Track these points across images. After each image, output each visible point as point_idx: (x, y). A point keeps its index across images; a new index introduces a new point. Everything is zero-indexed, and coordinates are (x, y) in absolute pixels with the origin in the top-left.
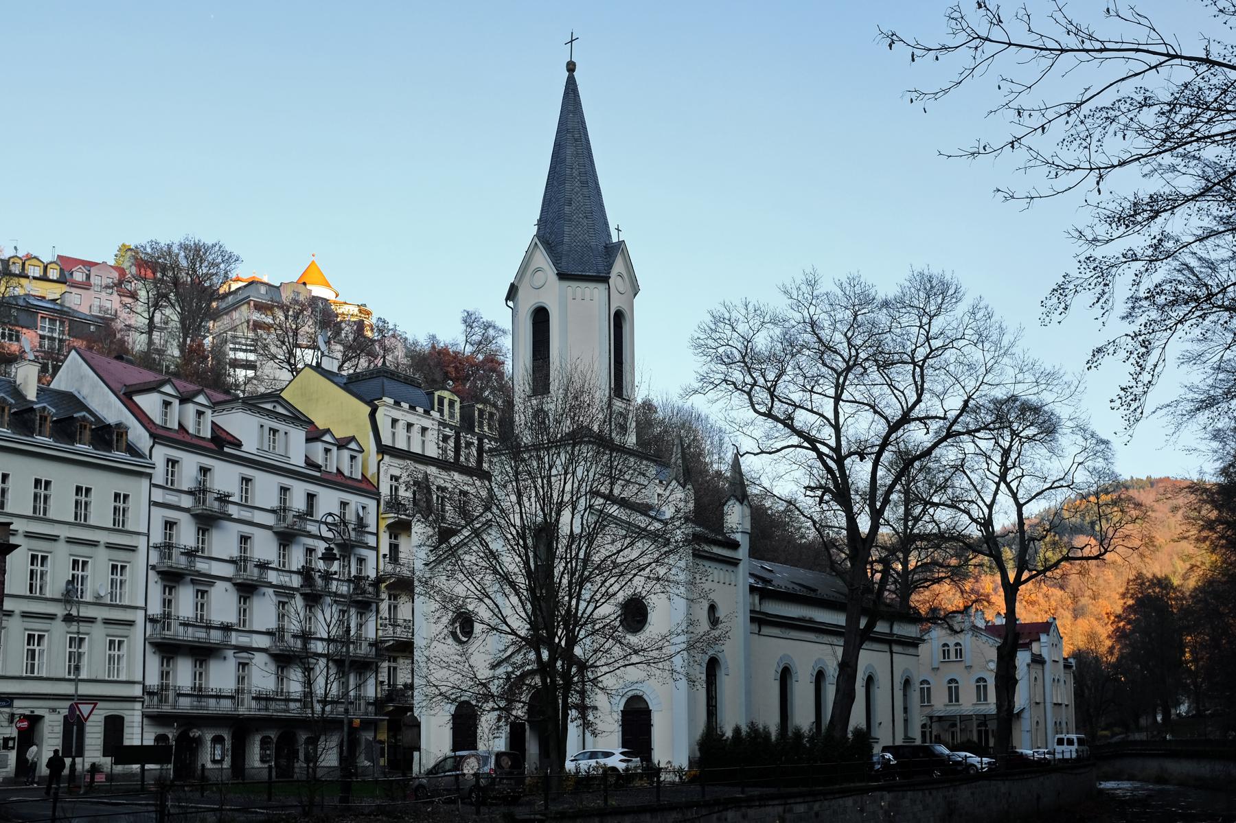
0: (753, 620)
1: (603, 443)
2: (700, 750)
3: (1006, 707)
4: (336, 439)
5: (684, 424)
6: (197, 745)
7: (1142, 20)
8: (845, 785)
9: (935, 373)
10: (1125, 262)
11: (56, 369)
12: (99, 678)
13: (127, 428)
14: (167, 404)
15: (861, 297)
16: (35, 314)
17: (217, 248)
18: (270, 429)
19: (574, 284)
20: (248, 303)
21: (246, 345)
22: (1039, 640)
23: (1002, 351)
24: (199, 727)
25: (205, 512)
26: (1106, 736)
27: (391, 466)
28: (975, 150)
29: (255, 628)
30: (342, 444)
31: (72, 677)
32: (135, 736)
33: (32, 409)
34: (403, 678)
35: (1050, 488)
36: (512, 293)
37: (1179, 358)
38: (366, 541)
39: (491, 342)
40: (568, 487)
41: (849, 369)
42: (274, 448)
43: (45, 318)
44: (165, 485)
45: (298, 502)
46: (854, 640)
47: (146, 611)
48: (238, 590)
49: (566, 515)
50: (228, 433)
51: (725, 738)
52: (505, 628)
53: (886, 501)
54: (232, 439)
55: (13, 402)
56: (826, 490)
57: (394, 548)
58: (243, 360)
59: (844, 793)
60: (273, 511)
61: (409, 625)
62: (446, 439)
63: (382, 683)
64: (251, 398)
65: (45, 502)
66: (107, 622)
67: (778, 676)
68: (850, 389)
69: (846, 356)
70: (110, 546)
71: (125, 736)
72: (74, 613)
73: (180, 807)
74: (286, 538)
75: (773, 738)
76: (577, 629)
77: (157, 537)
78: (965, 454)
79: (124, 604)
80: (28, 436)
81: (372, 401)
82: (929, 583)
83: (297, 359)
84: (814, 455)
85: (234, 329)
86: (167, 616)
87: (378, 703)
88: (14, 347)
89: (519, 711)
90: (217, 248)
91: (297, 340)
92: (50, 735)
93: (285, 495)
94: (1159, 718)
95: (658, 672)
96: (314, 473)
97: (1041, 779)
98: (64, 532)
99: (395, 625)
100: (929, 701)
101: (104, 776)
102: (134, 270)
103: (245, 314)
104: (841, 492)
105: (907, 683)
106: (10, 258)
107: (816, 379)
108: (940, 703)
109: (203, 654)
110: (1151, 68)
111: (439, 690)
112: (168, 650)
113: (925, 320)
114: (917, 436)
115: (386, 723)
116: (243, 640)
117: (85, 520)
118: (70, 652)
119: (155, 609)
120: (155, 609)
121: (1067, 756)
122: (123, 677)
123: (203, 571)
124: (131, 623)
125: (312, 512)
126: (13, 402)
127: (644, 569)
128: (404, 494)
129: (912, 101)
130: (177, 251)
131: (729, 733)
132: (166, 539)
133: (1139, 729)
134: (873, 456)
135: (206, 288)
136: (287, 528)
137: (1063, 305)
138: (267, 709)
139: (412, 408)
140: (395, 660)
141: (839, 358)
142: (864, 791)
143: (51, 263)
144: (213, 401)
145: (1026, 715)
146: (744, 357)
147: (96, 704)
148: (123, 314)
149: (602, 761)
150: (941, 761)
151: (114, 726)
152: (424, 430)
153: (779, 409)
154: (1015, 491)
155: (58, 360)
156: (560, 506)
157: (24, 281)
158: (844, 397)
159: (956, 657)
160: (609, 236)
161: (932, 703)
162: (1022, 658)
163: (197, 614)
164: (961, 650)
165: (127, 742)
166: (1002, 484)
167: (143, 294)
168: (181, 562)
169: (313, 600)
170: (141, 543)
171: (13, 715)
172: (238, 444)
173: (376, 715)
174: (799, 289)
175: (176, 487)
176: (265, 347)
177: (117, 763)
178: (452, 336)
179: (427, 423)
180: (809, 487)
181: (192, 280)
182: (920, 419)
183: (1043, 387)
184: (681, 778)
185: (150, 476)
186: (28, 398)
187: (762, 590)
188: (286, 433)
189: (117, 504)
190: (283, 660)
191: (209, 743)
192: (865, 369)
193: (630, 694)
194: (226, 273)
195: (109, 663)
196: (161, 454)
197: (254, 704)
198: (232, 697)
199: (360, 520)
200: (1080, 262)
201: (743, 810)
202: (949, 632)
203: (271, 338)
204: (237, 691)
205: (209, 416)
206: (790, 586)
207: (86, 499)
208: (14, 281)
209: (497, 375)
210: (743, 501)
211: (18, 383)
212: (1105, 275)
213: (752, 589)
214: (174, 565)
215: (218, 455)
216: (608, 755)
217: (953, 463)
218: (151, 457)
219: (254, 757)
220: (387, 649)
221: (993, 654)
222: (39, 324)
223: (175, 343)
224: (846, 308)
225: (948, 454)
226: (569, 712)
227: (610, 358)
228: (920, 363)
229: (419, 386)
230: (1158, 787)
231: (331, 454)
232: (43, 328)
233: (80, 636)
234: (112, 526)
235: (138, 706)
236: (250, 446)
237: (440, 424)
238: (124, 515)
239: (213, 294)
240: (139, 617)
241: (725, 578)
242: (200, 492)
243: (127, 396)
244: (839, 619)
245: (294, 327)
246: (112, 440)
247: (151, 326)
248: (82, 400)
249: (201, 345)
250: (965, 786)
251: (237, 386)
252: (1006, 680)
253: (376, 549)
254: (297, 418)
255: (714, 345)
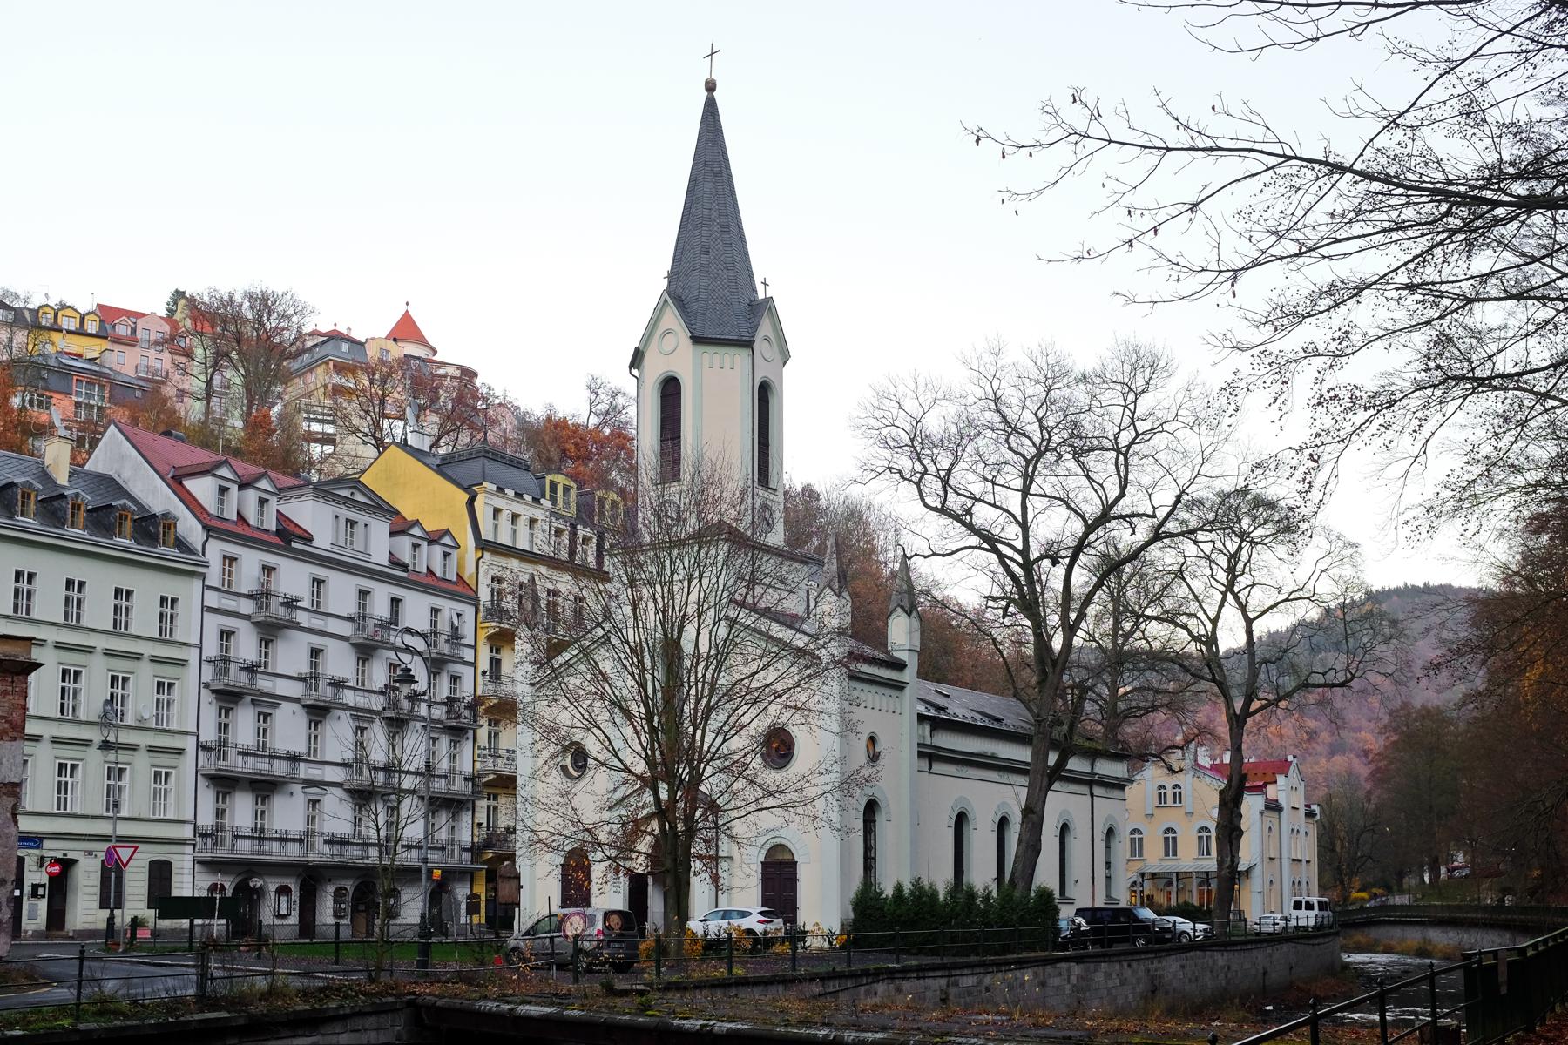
0: (921, 755)
1: (737, 540)
2: (854, 910)
3: (1228, 863)
4: (427, 533)
5: (852, 514)
6: (259, 898)
7: (1255, 118)
8: (1025, 955)
9: (1141, 462)
10: (1305, 358)
11: (94, 443)
12: (142, 816)
13: (176, 519)
14: (223, 490)
15: (1056, 369)
16: (70, 377)
17: (289, 296)
18: (347, 520)
19: (710, 349)
20: (327, 363)
21: (323, 414)
22: (1276, 782)
23: (1222, 437)
24: (260, 876)
25: (269, 619)
26: (1363, 899)
27: (491, 565)
28: (1080, 254)
29: (327, 759)
30: (433, 539)
31: (111, 814)
32: (185, 886)
33: (63, 496)
34: (503, 822)
35: (1287, 600)
36: (637, 360)
37: (1437, 448)
38: (461, 656)
39: (620, 412)
40: (693, 597)
41: (1040, 454)
42: (352, 544)
43: (81, 381)
44: (221, 587)
45: (380, 608)
46: (1045, 778)
47: (198, 736)
48: (307, 713)
49: (690, 630)
50: (296, 525)
51: (884, 896)
52: (616, 763)
53: (1082, 615)
54: (300, 533)
55: (41, 487)
56: (1011, 601)
57: (495, 664)
58: (318, 433)
59: (1022, 964)
60: (350, 619)
61: (511, 756)
62: (558, 532)
63: (480, 824)
64: (326, 483)
65: (79, 606)
66: (152, 750)
67: (953, 823)
68: (1038, 480)
69: (1037, 440)
70: (156, 660)
71: (174, 885)
72: (111, 739)
73: (224, 969)
74: (365, 652)
75: (941, 897)
76: (702, 765)
77: (212, 649)
78: (1185, 557)
79: (172, 728)
80: (57, 528)
81: (470, 487)
82: (1142, 712)
83: (384, 432)
84: (994, 557)
85: (309, 395)
86: (223, 743)
87: (475, 850)
88: (44, 418)
89: (640, 865)
90: (289, 296)
91: (383, 409)
92: (86, 883)
93: (365, 599)
94: (1427, 879)
95: (797, 818)
96: (398, 573)
97: (1269, 950)
98: (101, 643)
99: (496, 756)
100: (1141, 854)
101: (149, 932)
102: (188, 323)
103: (321, 377)
104: (1028, 601)
105: (1110, 832)
106: (40, 307)
107: (999, 467)
108: (1154, 859)
109: (264, 788)
110: (1268, 169)
111: (538, 836)
112: (224, 784)
113: (1131, 397)
114: (1125, 537)
115: (484, 872)
116: (313, 773)
117: (126, 629)
118: (108, 785)
119: (209, 735)
120: (209, 735)
121: (1302, 923)
122: (170, 816)
123: (266, 690)
124: (179, 752)
125: (397, 620)
126: (41, 487)
127: (780, 696)
128: (509, 604)
129: (1003, 202)
130: (240, 300)
131: (889, 892)
132: (222, 651)
133: (1401, 891)
134: (1067, 560)
135: (275, 346)
136: (367, 639)
137: (1233, 406)
138: (341, 856)
139: (519, 495)
140: (495, 798)
141: (1027, 442)
142: (1053, 961)
143: (89, 313)
144: (279, 486)
145: (1257, 872)
146: (912, 440)
147: (136, 847)
148: (176, 377)
149: (736, 922)
150: (1144, 928)
151: (160, 873)
152: (532, 521)
153: (955, 503)
154: (1244, 603)
155: (96, 432)
156: (683, 619)
157: (55, 336)
158: (1032, 491)
159: (1175, 802)
160: (755, 291)
161: (1145, 857)
162: (1251, 805)
163: (258, 741)
164: (1180, 793)
165: (175, 893)
166: (1229, 594)
167: (199, 352)
168: (238, 679)
169: (397, 725)
170: (192, 656)
171: (42, 858)
172: (308, 539)
173: (472, 863)
174: (979, 358)
175: (234, 589)
176: (346, 417)
177: (162, 916)
178: (575, 407)
179: (538, 514)
180: (990, 596)
181: (258, 335)
182: (1123, 517)
183: (1271, 480)
184: (830, 943)
185: (203, 576)
186: (59, 482)
187: (937, 722)
188: (366, 525)
189: (164, 610)
190: (362, 797)
191: (273, 894)
192: (1061, 456)
193: (768, 846)
194: (299, 327)
195: (155, 799)
196: (215, 550)
197: (326, 848)
198: (300, 841)
199: (455, 629)
200: (1253, 356)
201: (897, 982)
202: (1167, 771)
203: (352, 407)
204: (307, 834)
205: (274, 504)
206: (969, 714)
207: (127, 604)
208: (45, 335)
209: (625, 454)
210: (911, 612)
211: (46, 464)
212: (1283, 372)
213: (922, 718)
214: (232, 683)
215: (285, 551)
216: (744, 914)
217: (1170, 568)
218: (204, 554)
219: (326, 913)
220: (488, 784)
221: (1215, 799)
222: (75, 389)
223: (237, 413)
224: (1037, 382)
225: (1164, 557)
226: (692, 863)
227: (753, 439)
228: (1124, 450)
229: (527, 469)
230: (1417, 961)
231: (420, 552)
232: (79, 394)
233: (119, 766)
234: (157, 636)
235: (189, 849)
236: (323, 540)
237: (552, 514)
238: (171, 623)
239: (282, 353)
240: (190, 744)
241: (887, 705)
242: (261, 596)
243: (176, 481)
244: (1022, 754)
245: (381, 393)
246: (158, 533)
247: (209, 392)
248: (123, 485)
249: (267, 416)
250: (1174, 957)
251: (311, 463)
252: (1230, 831)
253: (474, 664)
254: (381, 508)
255: (877, 425)
